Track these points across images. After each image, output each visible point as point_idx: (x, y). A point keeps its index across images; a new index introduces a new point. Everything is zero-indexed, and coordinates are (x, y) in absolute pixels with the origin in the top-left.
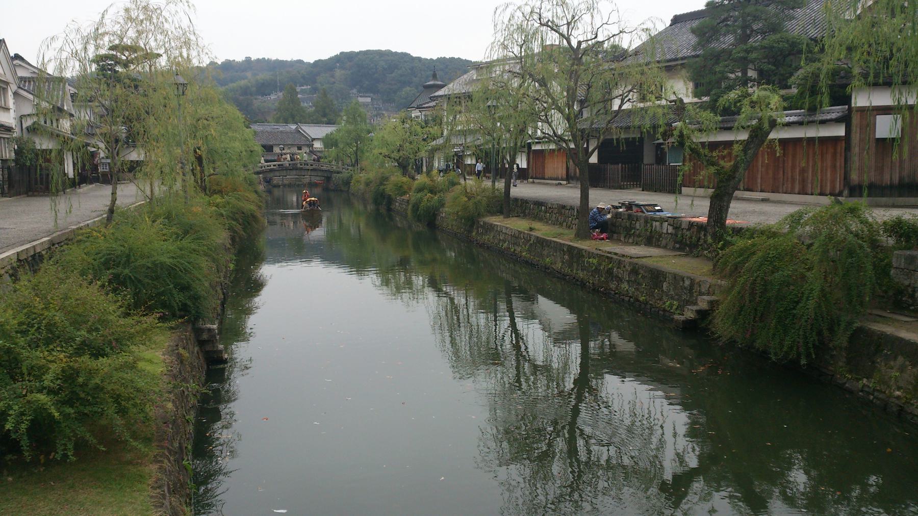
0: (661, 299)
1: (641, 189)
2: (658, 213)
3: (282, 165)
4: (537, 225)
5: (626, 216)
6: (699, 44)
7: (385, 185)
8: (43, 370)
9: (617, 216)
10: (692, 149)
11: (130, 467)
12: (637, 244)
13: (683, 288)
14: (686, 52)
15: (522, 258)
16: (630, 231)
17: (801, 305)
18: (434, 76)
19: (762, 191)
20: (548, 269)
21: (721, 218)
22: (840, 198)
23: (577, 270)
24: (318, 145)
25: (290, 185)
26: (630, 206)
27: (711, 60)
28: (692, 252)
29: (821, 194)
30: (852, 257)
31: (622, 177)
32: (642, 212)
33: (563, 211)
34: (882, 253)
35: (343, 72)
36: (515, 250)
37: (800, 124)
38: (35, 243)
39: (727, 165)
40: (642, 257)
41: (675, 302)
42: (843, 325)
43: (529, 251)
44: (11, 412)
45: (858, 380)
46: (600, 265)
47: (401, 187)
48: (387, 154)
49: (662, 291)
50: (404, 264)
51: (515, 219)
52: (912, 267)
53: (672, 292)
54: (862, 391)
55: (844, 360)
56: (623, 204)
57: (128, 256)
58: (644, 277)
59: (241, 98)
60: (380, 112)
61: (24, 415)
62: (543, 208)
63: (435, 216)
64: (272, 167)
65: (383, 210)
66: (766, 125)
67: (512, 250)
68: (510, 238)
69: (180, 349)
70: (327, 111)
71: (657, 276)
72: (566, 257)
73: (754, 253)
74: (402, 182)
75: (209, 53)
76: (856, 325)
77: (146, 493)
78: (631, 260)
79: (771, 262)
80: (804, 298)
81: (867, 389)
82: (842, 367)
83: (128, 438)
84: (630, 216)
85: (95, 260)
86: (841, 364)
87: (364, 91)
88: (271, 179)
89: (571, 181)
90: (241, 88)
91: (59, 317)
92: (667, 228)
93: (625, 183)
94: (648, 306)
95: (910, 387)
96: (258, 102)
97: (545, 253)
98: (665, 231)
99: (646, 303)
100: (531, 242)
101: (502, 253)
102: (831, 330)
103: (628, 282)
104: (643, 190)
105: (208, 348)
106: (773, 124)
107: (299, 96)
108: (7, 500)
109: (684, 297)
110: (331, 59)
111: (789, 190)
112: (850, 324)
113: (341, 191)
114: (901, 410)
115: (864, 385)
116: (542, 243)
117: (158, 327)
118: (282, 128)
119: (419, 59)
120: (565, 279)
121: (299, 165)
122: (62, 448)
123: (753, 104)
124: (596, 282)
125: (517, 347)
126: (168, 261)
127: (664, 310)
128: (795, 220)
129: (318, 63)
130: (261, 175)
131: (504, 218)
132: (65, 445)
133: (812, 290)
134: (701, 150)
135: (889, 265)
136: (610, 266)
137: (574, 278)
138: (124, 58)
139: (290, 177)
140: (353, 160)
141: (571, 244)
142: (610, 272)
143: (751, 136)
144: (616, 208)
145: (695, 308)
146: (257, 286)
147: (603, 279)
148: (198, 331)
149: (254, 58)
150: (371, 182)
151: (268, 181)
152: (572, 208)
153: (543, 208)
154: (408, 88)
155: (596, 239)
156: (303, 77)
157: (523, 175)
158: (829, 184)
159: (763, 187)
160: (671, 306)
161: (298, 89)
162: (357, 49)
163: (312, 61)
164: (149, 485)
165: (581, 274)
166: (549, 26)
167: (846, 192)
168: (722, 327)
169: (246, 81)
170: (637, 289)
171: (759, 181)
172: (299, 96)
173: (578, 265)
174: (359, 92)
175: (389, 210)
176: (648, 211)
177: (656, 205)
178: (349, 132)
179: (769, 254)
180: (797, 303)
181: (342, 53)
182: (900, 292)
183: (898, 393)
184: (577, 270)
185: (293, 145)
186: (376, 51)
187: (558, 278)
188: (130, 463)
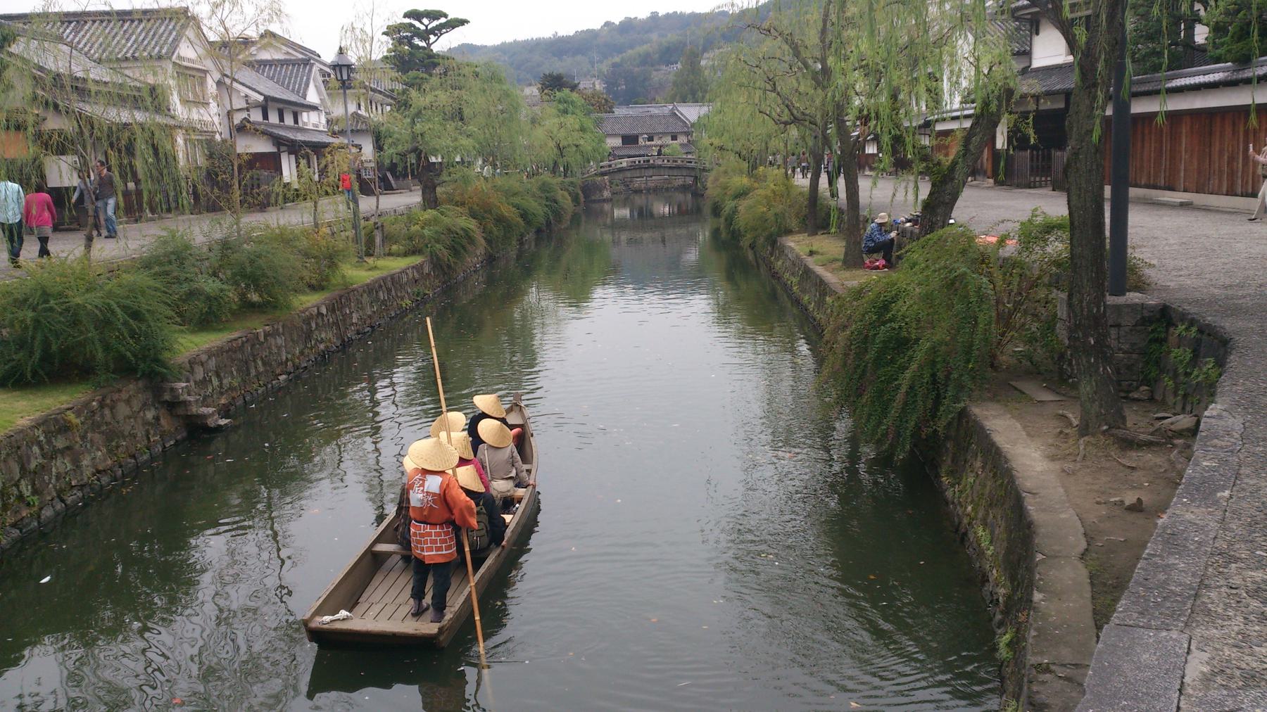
59: (636, 69)
89: (977, 177)
90: (640, 55)
93: (1038, 179)
104: (1054, 190)
111: (1216, 188)
130: (606, 177)
138: (423, 28)
149: (662, 13)
171: (1182, 174)
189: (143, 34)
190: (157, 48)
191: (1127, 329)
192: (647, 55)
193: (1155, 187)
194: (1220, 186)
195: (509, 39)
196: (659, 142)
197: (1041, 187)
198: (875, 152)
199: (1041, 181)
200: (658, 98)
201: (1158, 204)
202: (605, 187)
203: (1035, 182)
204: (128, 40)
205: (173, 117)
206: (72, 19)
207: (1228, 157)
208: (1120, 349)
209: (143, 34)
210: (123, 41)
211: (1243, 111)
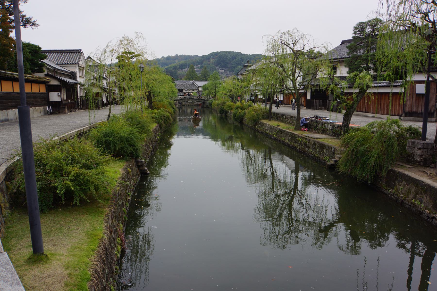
0: (323, 156)
1: (327, 110)
2: (327, 121)
3: (186, 97)
4: (281, 124)
5: (315, 122)
6: (349, 53)
7: (224, 106)
8: (70, 173)
9: (312, 121)
10: (337, 95)
11: (99, 209)
12: (319, 133)
13: (331, 151)
14: (345, 56)
15: (274, 137)
16: (316, 128)
17: (370, 160)
18: (248, 62)
19: (372, 113)
20: (283, 142)
21: (348, 123)
22: (401, 117)
23: (294, 143)
24: (200, 89)
25: (189, 105)
26: (317, 118)
27: (354, 59)
28: (338, 137)
29: (395, 115)
30: (390, 141)
31: (320, 104)
32: (321, 120)
33: (292, 118)
34: (404, 140)
35: (213, 60)
36: (271, 134)
37: (388, 86)
38: (84, 128)
39: (350, 102)
40: (318, 139)
41: (328, 157)
42: (385, 168)
43: (277, 134)
44: (59, 187)
45: (389, 190)
46: (302, 141)
47: (230, 107)
48: (225, 93)
49: (324, 152)
50: (231, 138)
51: (273, 121)
52: (413, 146)
53: (327, 153)
54: (390, 194)
55: (385, 182)
56: (314, 116)
57: (112, 133)
58: (317, 147)
59: (173, 70)
60: (228, 76)
61: (63, 188)
62: (284, 117)
63: (242, 119)
64: (182, 98)
65: (224, 116)
66: (365, 87)
67: (270, 134)
68: (270, 129)
69: (128, 168)
70: (206, 75)
71: (322, 146)
72: (290, 137)
73: (354, 138)
74: (231, 105)
75: (154, 55)
76: (389, 168)
77: (103, 218)
78: (314, 140)
79: (360, 142)
80: (372, 157)
81: (391, 193)
82: (384, 185)
83: (97, 198)
84: (316, 121)
85: (101, 134)
86: (383, 183)
87: (222, 67)
88: (182, 103)
90: (173, 66)
91: (76, 155)
92: (330, 127)
94: (319, 159)
95: (406, 193)
96: (179, 72)
97: (283, 135)
98: (329, 128)
99: (318, 157)
100: (278, 131)
101: (267, 135)
102: (381, 170)
103: (312, 148)
104: (327, 111)
105: (141, 168)
106: (368, 87)
107: (195, 69)
108: (58, 216)
109: (331, 155)
110: (209, 55)
111: (382, 113)
112: (387, 167)
113: (209, 108)
114: (402, 202)
115: (391, 192)
116: (281, 131)
117: (112, 160)
118: (187, 82)
119: (244, 55)
120: (289, 147)
121: (192, 97)
122: (76, 200)
123: (360, 78)
124: (300, 148)
125: (272, 173)
126: (126, 135)
127: (324, 160)
128: (371, 125)
129: (203, 56)
130: (177, 101)
131: (269, 120)
132: (77, 199)
133: (374, 154)
134: (340, 96)
135: (406, 145)
136: (306, 142)
137: (293, 146)
139: (189, 102)
140: (214, 95)
141: (292, 132)
142: (305, 144)
143: (359, 91)
144: (312, 118)
145: (334, 160)
146: (169, 146)
147: (303, 147)
148: (137, 162)
150: (219, 104)
151: (181, 104)
152: (295, 117)
153: (284, 117)
154: (240, 66)
155: (303, 130)
156: (198, 62)
157: (281, 103)
158: (397, 111)
159: (373, 111)
160: (327, 158)
161: (195, 67)
162: (219, 51)
163: (201, 56)
164: (104, 215)
165: (295, 145)
166: (285, 44)
167: (403, 115)
168: (342, 168)
169: (175, 64)
170: (315, 151)
171: (371, 109)
172: (195, 69)
173: (294, 141)
174: (220, 67)
175: (226, 116)
176: (323, 120)
177: (327, 117)
178: (213, 84)
179: (359, 139)
180: (369, 159)
181: (213, 52)
182: (409, 156)
183: (402, 195)
184: (294, 143)
185: (191, 89)
186: (227, 51)
187: (287, 146)
188: (100, 207)
189: (69, 57)
190: (74, 61)
191: (430, 149)
192: (176, 66)
193: (362, 112)
194: (384, 112)
195: (32, 43)
196: (189, 92)
197: (322, 110)
198: (261, 97)
199: (322, 108)
200: (183, 79)
201: (363, 116)
202: (177, 104)
203: (320, 108)
204: (65, 58)
205: (78, 81)
206: (47, 52)
207: (386, 105)
208: (428, 154)
209: (69, 57)
210: (63, 59)
211: (388, 93)
